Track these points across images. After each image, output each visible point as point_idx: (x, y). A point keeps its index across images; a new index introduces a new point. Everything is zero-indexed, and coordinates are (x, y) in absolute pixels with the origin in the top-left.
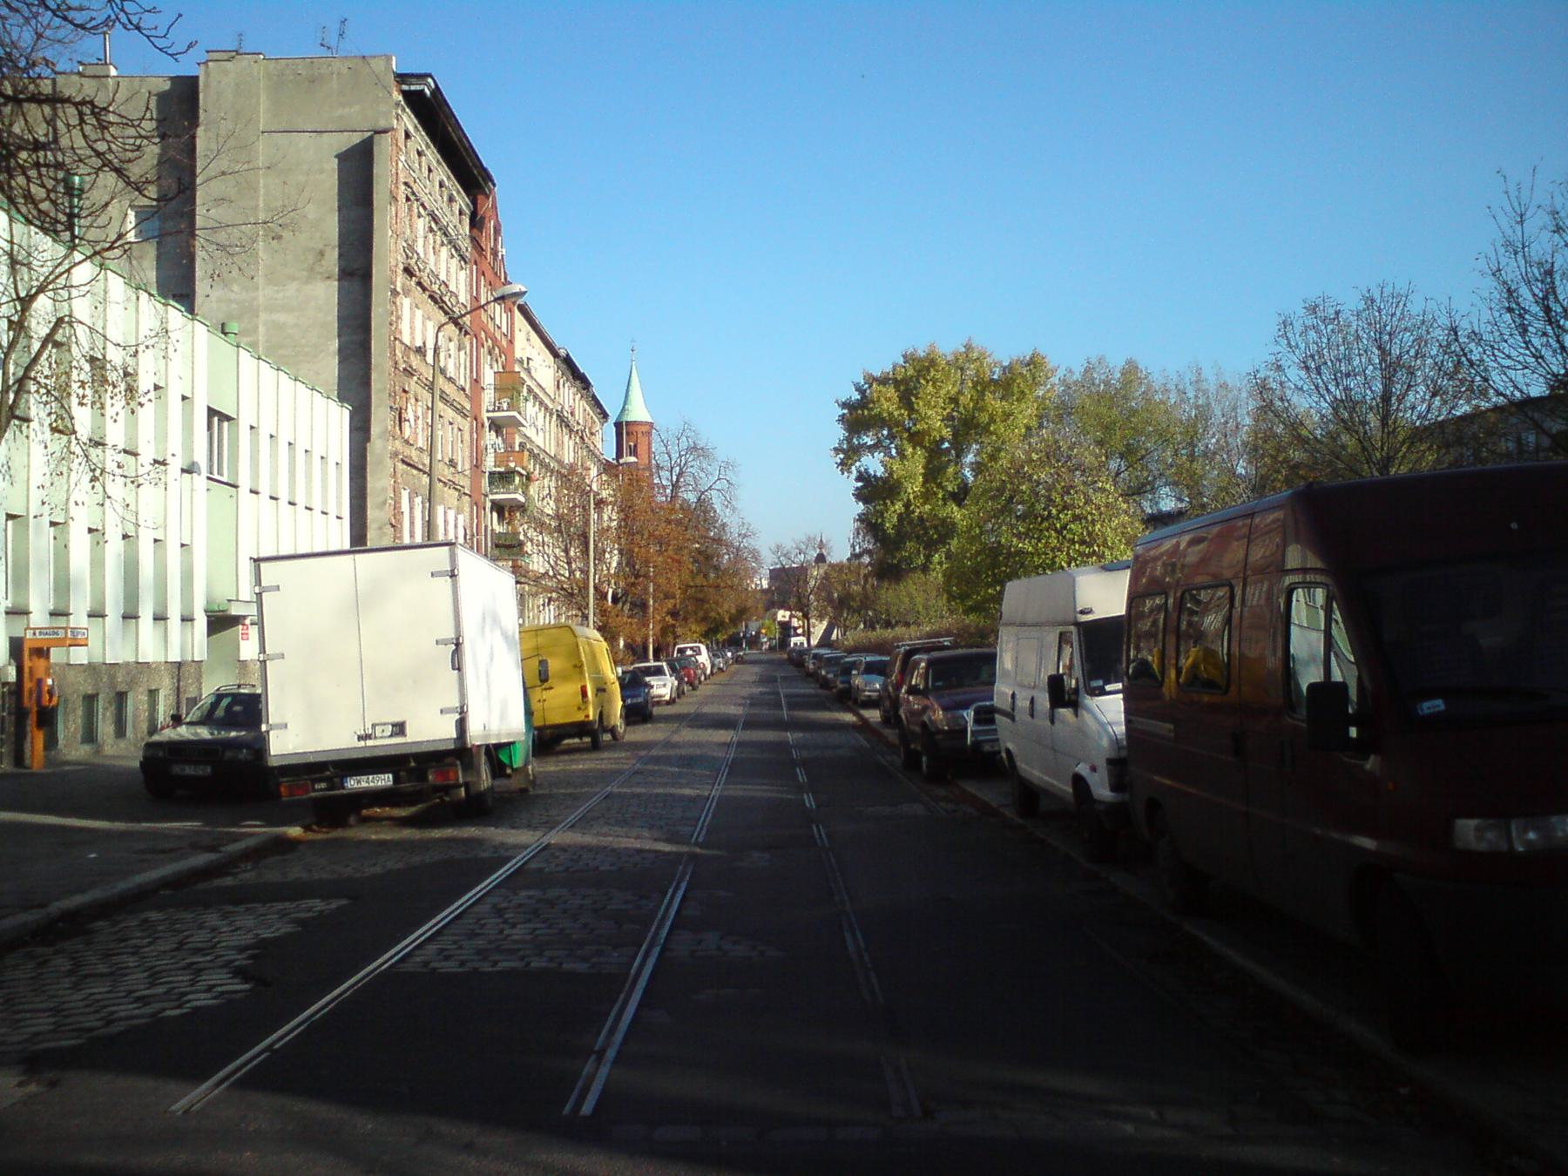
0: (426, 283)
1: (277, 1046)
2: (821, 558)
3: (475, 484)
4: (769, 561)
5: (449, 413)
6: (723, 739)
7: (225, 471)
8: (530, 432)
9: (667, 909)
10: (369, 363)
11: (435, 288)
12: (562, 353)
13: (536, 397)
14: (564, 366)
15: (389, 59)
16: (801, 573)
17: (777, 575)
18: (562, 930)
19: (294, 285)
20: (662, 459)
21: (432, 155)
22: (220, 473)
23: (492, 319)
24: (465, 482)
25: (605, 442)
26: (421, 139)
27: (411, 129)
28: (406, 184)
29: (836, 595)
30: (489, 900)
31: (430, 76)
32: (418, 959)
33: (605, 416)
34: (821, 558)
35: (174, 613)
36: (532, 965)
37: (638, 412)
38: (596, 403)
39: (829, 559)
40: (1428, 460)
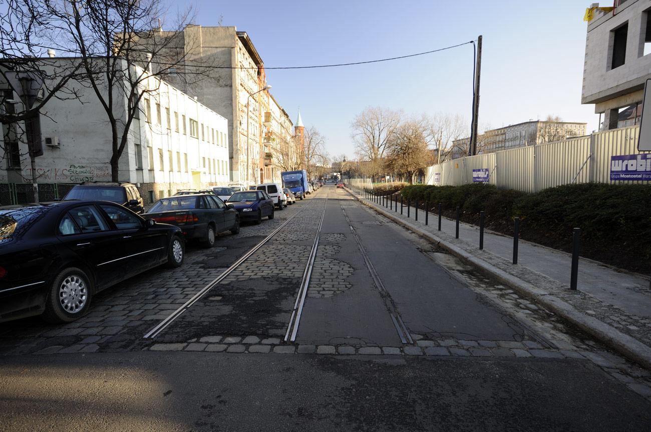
0: (246, 88)
1: (188, 306)
2: (344, 161)
3: (260, 140)
4: (333, 161)
5: (253, 122)
6: (600, 363)
7: (195, 134)
8: (274, 128)
9: (313, 253)
10: (232, 109)
11: (249, 90)
12: (282, 108)
13: (275, 119)
14: (282, 112)
15: (234, 28)
16: (340, 164)
17: (334, 164)
18: (283, 259)
19: (212, 88)
20: (307, 135)
21: (247, 55)
22: (194, 135)
23: (264, 99)
24: (258, 140)
25: (292, 130)
26: (244, 49)
27: (241, 47)
28: (240, 62)
29: (80, 214)
30: (261, 249)
31: (245, 32)
32: (240, 269)
33: (292, 124)
34: (344, 161)
35: (217, 173)
36: (274, 272)
37: (301, 124)
38: (290, 121)
39: (346, 161)
40: (608, 120)
